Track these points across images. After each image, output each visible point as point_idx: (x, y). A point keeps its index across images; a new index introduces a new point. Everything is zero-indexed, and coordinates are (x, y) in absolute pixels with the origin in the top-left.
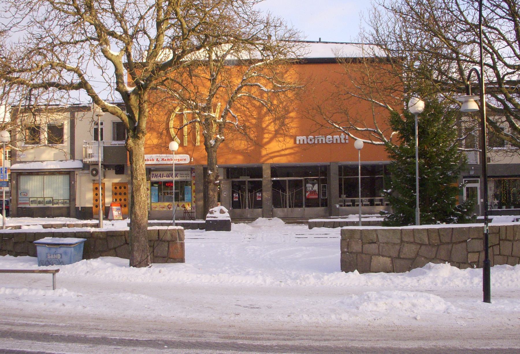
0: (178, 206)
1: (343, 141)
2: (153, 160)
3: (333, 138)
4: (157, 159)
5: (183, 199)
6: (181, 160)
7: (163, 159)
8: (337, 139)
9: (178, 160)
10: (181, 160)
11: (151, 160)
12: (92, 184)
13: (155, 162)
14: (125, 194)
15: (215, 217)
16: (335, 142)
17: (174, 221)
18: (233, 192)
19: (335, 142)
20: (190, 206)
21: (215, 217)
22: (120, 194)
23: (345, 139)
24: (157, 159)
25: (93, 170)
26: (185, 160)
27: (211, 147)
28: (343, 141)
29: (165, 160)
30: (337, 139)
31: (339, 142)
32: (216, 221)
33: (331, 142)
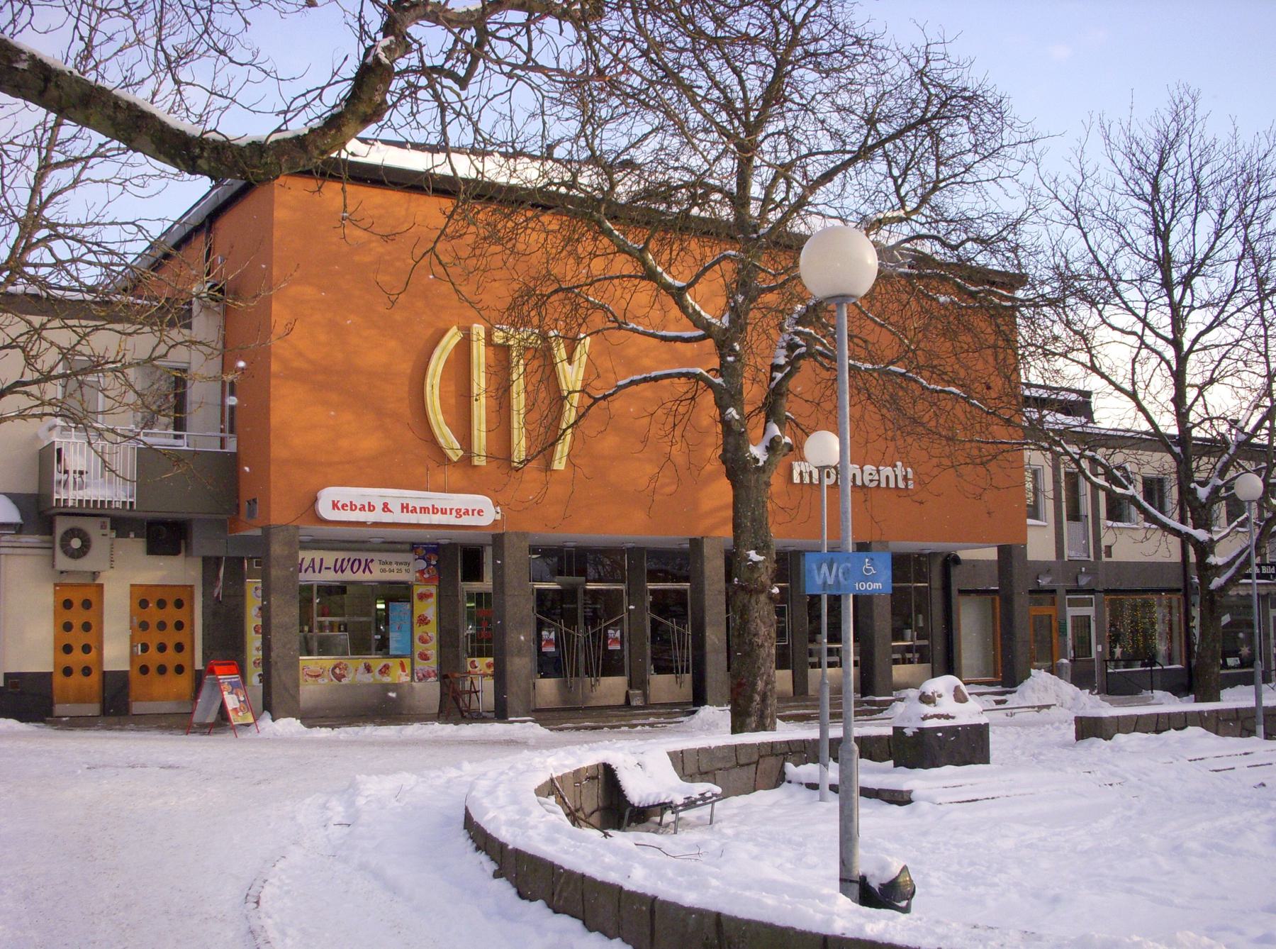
0: (368, 669)
1: (901, 485)
2: (371, 508)
3: (878, 471)
4: (385, 505)
5: (383, 646)
6: (467, 512)
7: (405, 508)
8: (887, 477)
9: (458, 511)
10: (467, 512)
11: (363, 508)
12: (50, 589)
13: (378, 516)
14: (179, 626)
15: (947, 717)
16: (883, 485)
17: (847, 730)
18: (540, 626)
19: (883, 485)
20: (408, 670)
21: (947, 717)
22: (162, 626)
23: (905, 478)
24: (385, 505)
25: (72, 533)
26: (480, 512)
27: (758, 469)
28: (901, 485)
29: (414, 510)
30: (887, 477)
31: (892, 485)
32: (953, 730)
33: (875, 484)
